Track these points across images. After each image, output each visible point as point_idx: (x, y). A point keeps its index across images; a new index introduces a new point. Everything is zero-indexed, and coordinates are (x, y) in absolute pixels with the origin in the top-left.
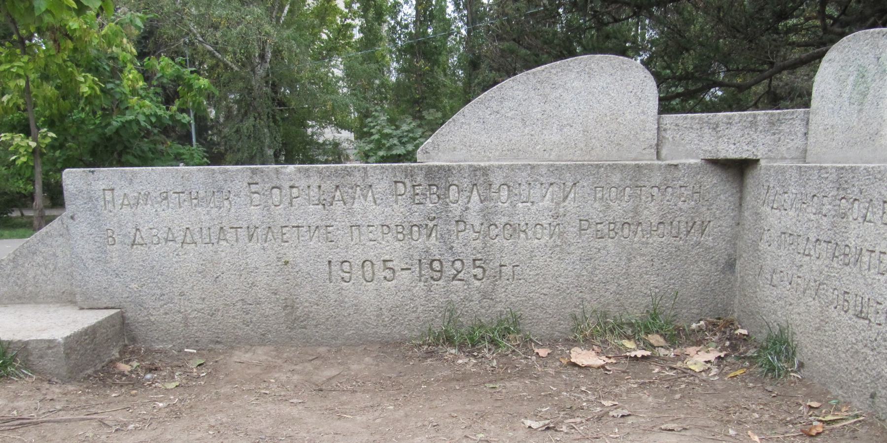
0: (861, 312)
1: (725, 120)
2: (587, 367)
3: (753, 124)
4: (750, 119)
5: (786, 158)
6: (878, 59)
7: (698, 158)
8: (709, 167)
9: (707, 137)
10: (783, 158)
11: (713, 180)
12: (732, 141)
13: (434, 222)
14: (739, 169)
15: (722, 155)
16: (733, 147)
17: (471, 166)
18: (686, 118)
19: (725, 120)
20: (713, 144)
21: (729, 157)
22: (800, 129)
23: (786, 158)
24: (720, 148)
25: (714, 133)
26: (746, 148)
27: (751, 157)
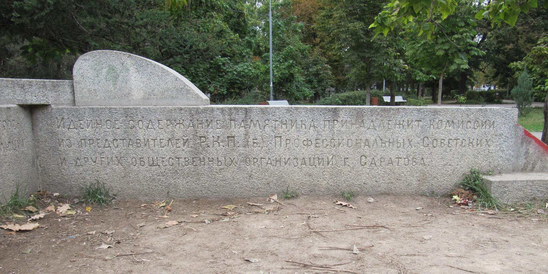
0: (153, 163)
1: (28, 83)
2: (34, 229)
3: (44, 86)
4: (42, 83)
5: (64, 104)
6: (123, 64)
7: (14, 104)
8: (20, 109)
9: (18, 92)
10: (63, 104)
11: (22, 116)
12: (34, 95)
13: (187, 138)
14: (31, 110)
15: (29, 102)
16: (35, 98)
17: (179, 108)
18: (3, 80)
19: (28, 83)
20: (23, 96)
21: (33, 103)
22: (69, 90)
23: (64, 104)
24: (27, 98)
25: (22, 90)
26: (42, 98)
27: (46, 103)
